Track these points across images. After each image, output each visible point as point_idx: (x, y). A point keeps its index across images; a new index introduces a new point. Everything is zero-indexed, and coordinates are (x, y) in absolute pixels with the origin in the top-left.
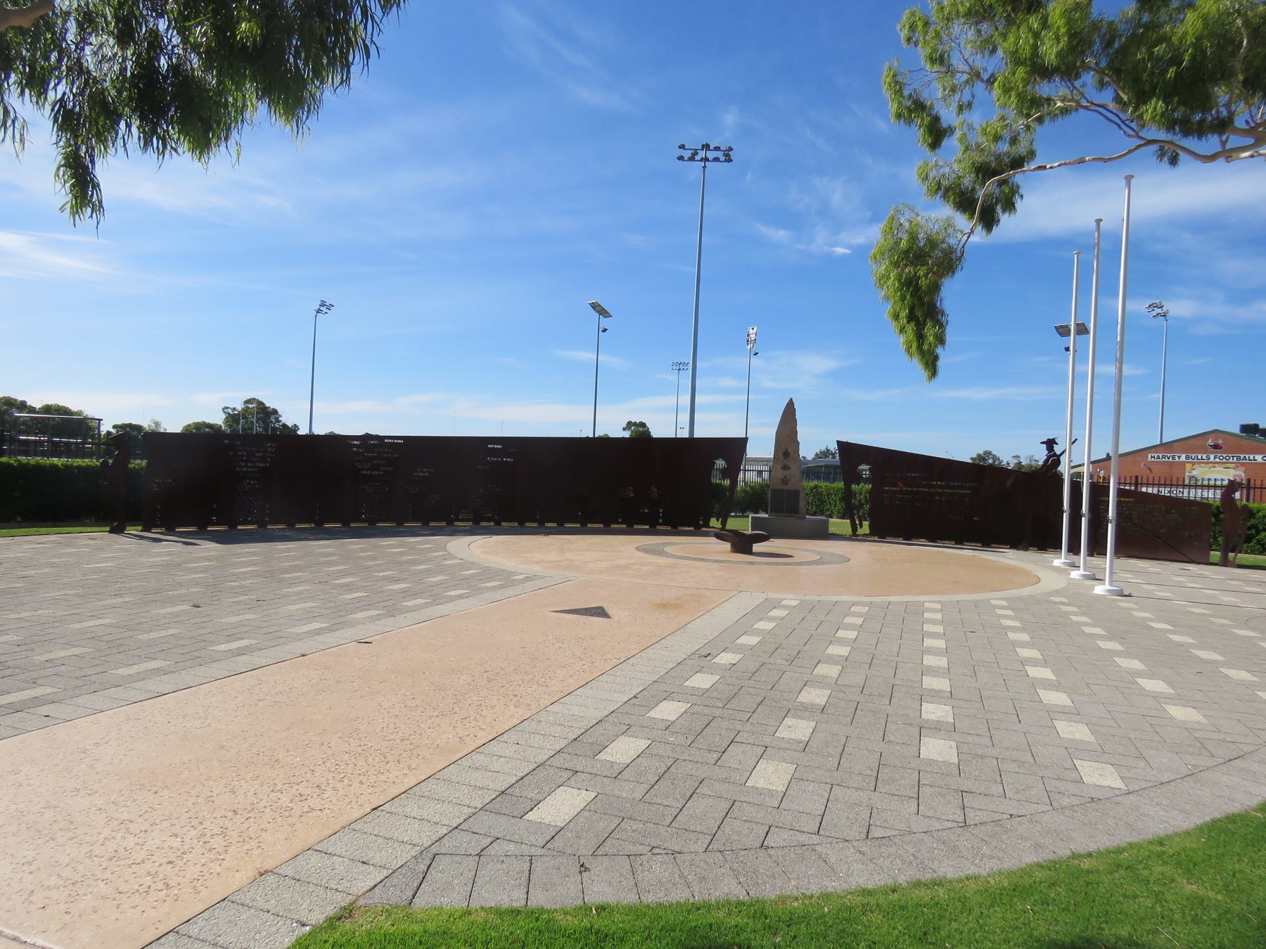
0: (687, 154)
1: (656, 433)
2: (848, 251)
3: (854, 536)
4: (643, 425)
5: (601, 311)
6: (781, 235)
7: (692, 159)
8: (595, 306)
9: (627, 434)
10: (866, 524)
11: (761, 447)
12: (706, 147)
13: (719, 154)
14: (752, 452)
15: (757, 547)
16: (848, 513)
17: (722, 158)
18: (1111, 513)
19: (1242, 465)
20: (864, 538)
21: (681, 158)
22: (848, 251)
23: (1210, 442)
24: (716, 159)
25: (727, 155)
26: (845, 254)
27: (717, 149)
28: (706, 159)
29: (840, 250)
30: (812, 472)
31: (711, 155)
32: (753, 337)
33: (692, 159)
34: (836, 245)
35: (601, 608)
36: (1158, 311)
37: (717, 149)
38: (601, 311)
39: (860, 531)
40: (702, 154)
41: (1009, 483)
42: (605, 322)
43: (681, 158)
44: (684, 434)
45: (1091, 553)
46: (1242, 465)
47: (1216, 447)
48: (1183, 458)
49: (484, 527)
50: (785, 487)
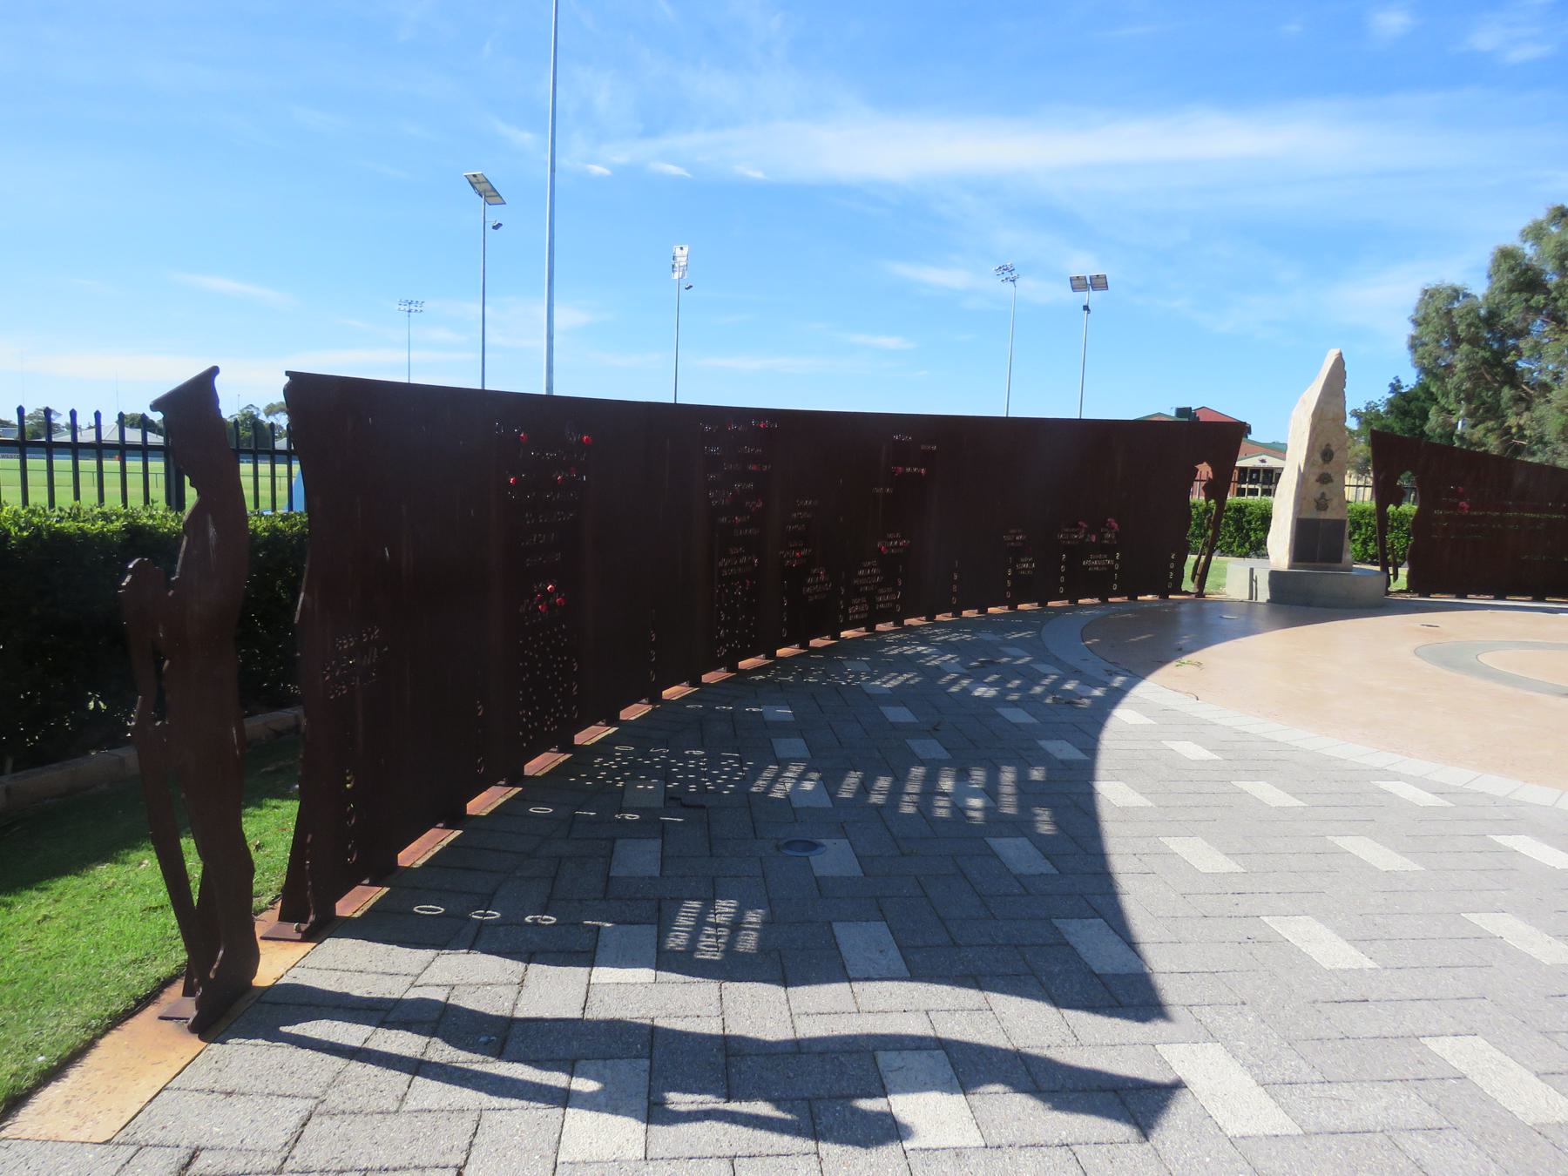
2: (606, 172)
10: (1403, 572)
29: (597, 170)
32: (682, 261)
36: (1007, 274)
42: (495, 213)
50: (1323, 515)
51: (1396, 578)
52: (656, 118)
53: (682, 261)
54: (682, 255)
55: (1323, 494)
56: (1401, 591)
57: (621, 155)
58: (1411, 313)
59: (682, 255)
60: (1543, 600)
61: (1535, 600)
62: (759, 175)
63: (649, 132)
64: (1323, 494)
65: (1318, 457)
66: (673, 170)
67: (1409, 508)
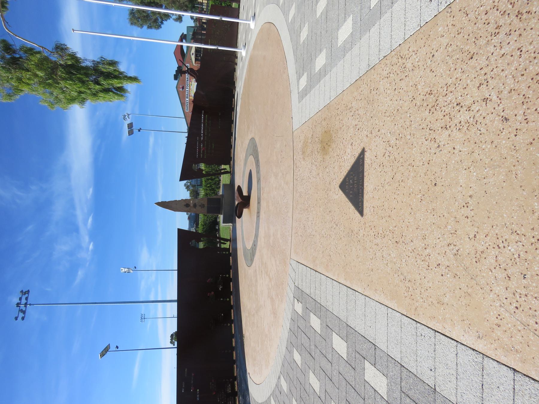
0: (21, 315)
1: (175, 329)
2: (92, 244)
3: (232, 173)
4: (172, 336)
5: (107, 350)
6: (80, 273)
7: (24, 312)
8: (103, 355)
9: (176, 343)
10: (223, 167)
11: (182, 221)
12: (18, 305)
13: (24, 298)
14: (185, 226)
15: (245, 193)
16: (220, 173)
17: (27, 295)
18: (217, 18)
19: (190, 79)
20: (233, 168)
21: (23, 318)
22: (92, 244)
23: (181, 90)
24: (27, 299)
25: (25, 293)
26: (93, 245)
27: (20, 299)
28: (26, 304)
29: (91, 247)
30: (195, 194)
31: (24, 301)
32: (126, 270)
33: (24, 312)
34: (88, 248)
35: (343, 186)
36: (127, 117)
37: (20, 299)
38: (107, 350)
39: (228, 170)
40: (22, 307)
41: (202, 93)
42: (113, 348)
43: (23, 318)
44: (176, 304)
45: (237, 17)
46: (190, 79)
47: (183, 88)
48: (188, 99)
49: (239, 385)
50: (206, 206)
51: (226, 169)
52: (71, 228)
53: (126, 270)
54: (124, 270)
55: (200, 206)
56: (230, 167)
57: (85, 238)
58: (139, 28)
59: (124, 270)
60: (233, 121)
61: (232, 148)
62: (91, 190)
63: (77, 230)
64: (200, 206)
65: (188, 208)
66: (90, 220)
67: (202, 166)
